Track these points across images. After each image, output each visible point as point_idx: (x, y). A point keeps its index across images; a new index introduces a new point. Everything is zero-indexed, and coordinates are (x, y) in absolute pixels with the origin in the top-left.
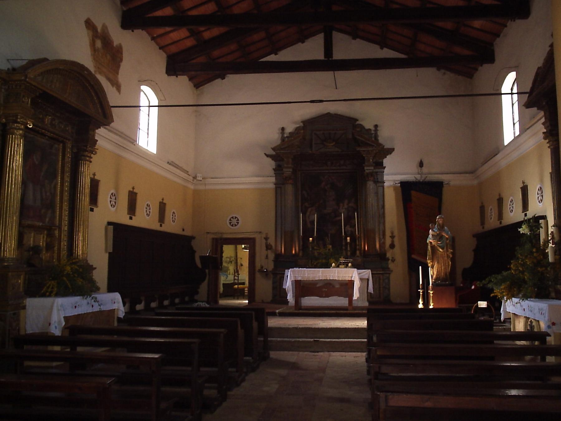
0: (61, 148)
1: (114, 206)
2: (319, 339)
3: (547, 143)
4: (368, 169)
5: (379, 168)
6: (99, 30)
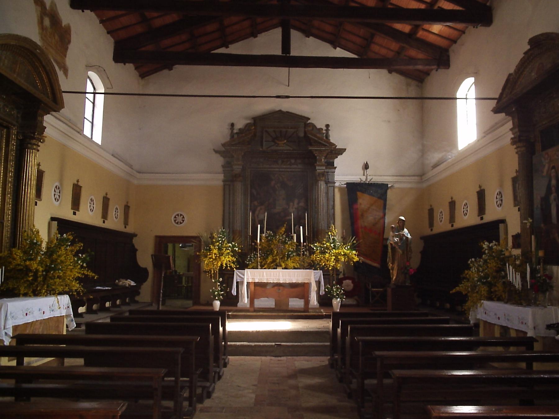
0: (5, 133)
1: (58, 200)
2: (281, 343)
3: (515, 149)
4: (320, 169)
6: (48, 6)
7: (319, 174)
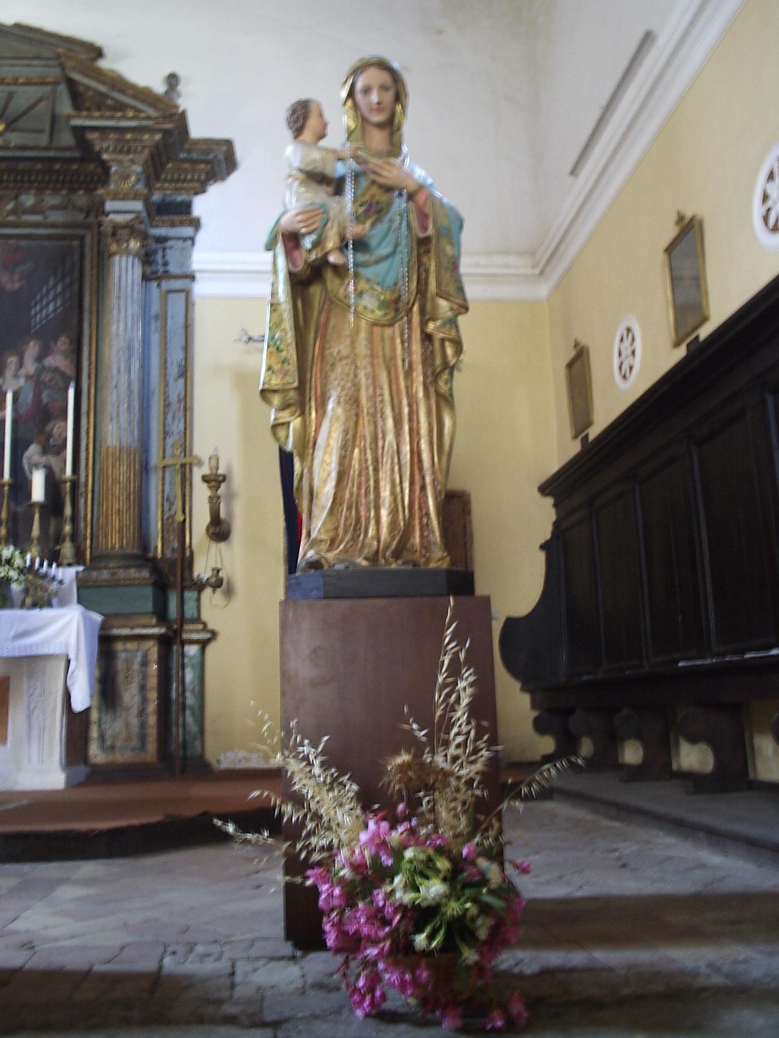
5: (173, 225)
7: (116, 227)
